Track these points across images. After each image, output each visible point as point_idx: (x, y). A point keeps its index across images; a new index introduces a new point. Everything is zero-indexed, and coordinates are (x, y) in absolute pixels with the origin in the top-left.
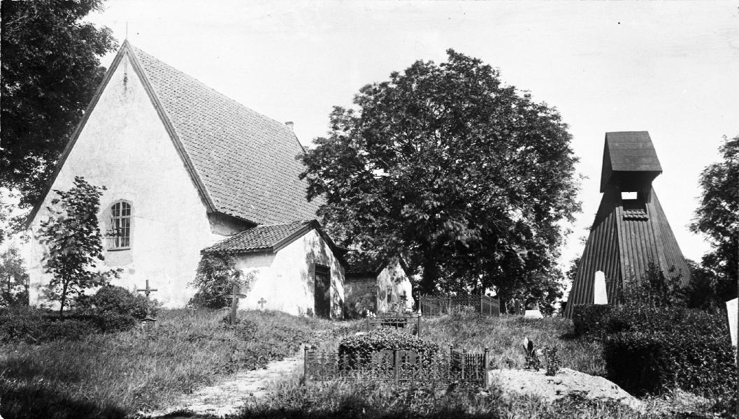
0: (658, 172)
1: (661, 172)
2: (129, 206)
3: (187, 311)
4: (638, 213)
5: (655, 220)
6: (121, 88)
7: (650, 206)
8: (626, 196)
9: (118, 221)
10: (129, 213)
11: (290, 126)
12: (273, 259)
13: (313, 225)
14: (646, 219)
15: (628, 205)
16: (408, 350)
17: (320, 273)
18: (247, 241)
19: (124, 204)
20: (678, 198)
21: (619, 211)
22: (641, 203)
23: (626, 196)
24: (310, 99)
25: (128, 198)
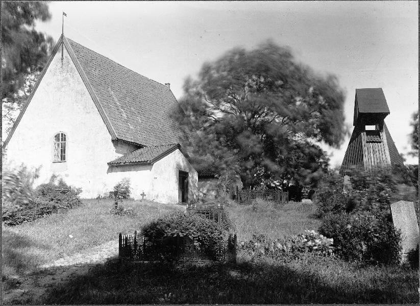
0: (386, 114)
1: (389, 113)
2: (65, 136)
3: (298, 130)
4: (376, 139)
5: (385, 141)
6: (60, 65)
7: (383, 135)
8: (368, 128)
9: (58, 145)
10: (65, 140)
11: (167, 86)
12: (151, 168)
13: (179, 146)
14: (380, 142)
15: (369, 133)
16: (277, 100)
17: (183, 177)
18: (136, 156)
19: (62, 134)
20: (399, 127)
21: (364, 136)
22: (376, 133)
23: (368, 128)
24: (173, 67)
25: (65, 131)
